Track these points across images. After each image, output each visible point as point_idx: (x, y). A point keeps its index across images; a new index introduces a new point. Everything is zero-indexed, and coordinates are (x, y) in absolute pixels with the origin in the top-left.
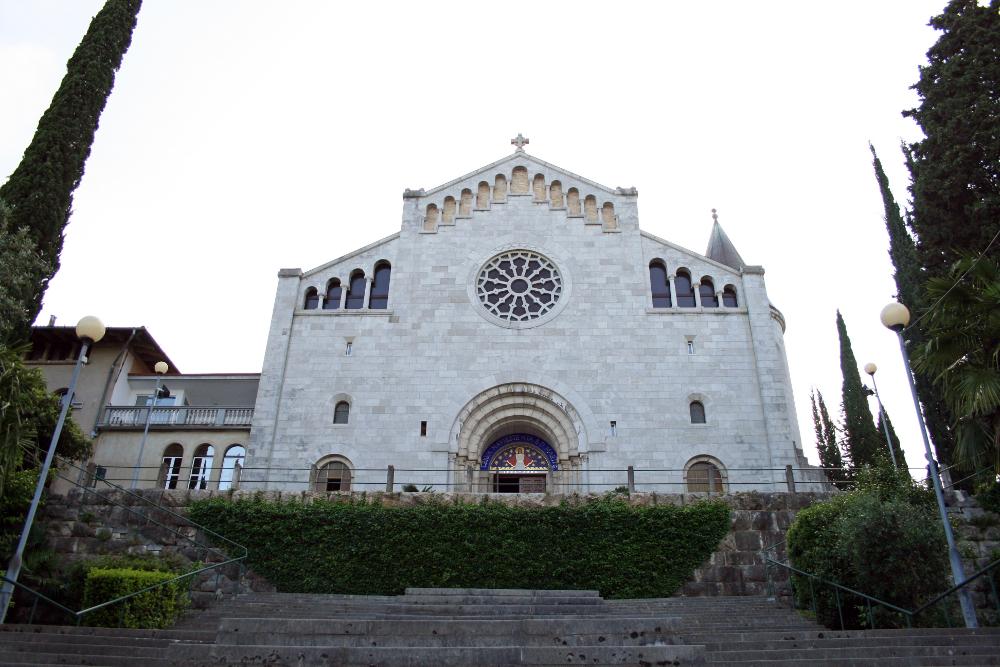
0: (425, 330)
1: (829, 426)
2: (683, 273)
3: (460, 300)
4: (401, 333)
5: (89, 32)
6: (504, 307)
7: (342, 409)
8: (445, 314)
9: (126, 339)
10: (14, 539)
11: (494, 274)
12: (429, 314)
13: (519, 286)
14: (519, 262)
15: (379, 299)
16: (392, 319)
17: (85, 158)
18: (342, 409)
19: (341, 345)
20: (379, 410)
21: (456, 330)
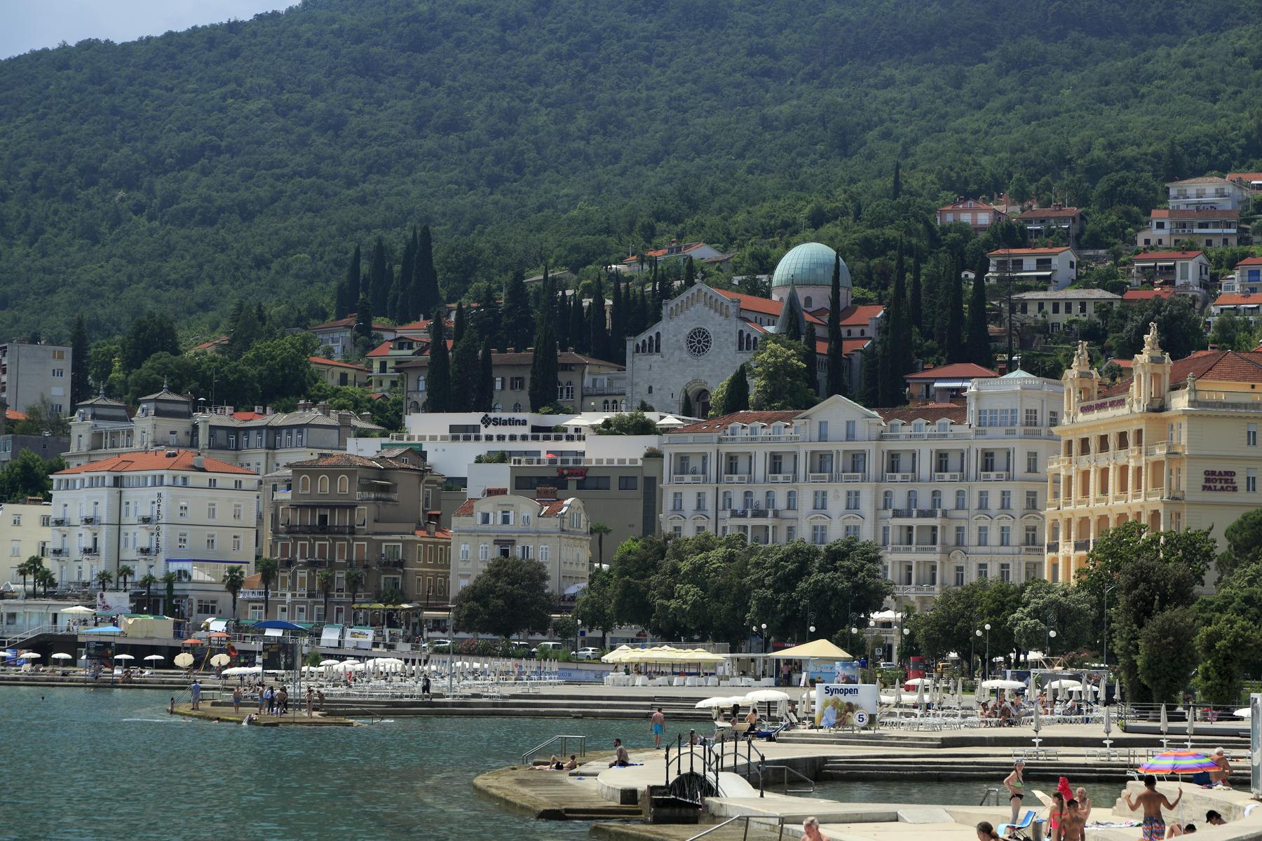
0: (671, 361)
1: (607, 423)
2: (749, 335)
3: (681, 349)
4: (664, 362)
5: (969, 361)
6: (703, 350)
7: (650, 389)
8: (677, 353)
9: (1155, 272)
10: (785, 664)
11: (691, 347)
12: (672, 354)
13: (699, 342)
14: (690, 342)
15: (658, 350)
16: (662, 356)
17: (179, 35)
18: (650, 389)
19: (648, 367)
20: (660, 389)
21: (681, 360)
